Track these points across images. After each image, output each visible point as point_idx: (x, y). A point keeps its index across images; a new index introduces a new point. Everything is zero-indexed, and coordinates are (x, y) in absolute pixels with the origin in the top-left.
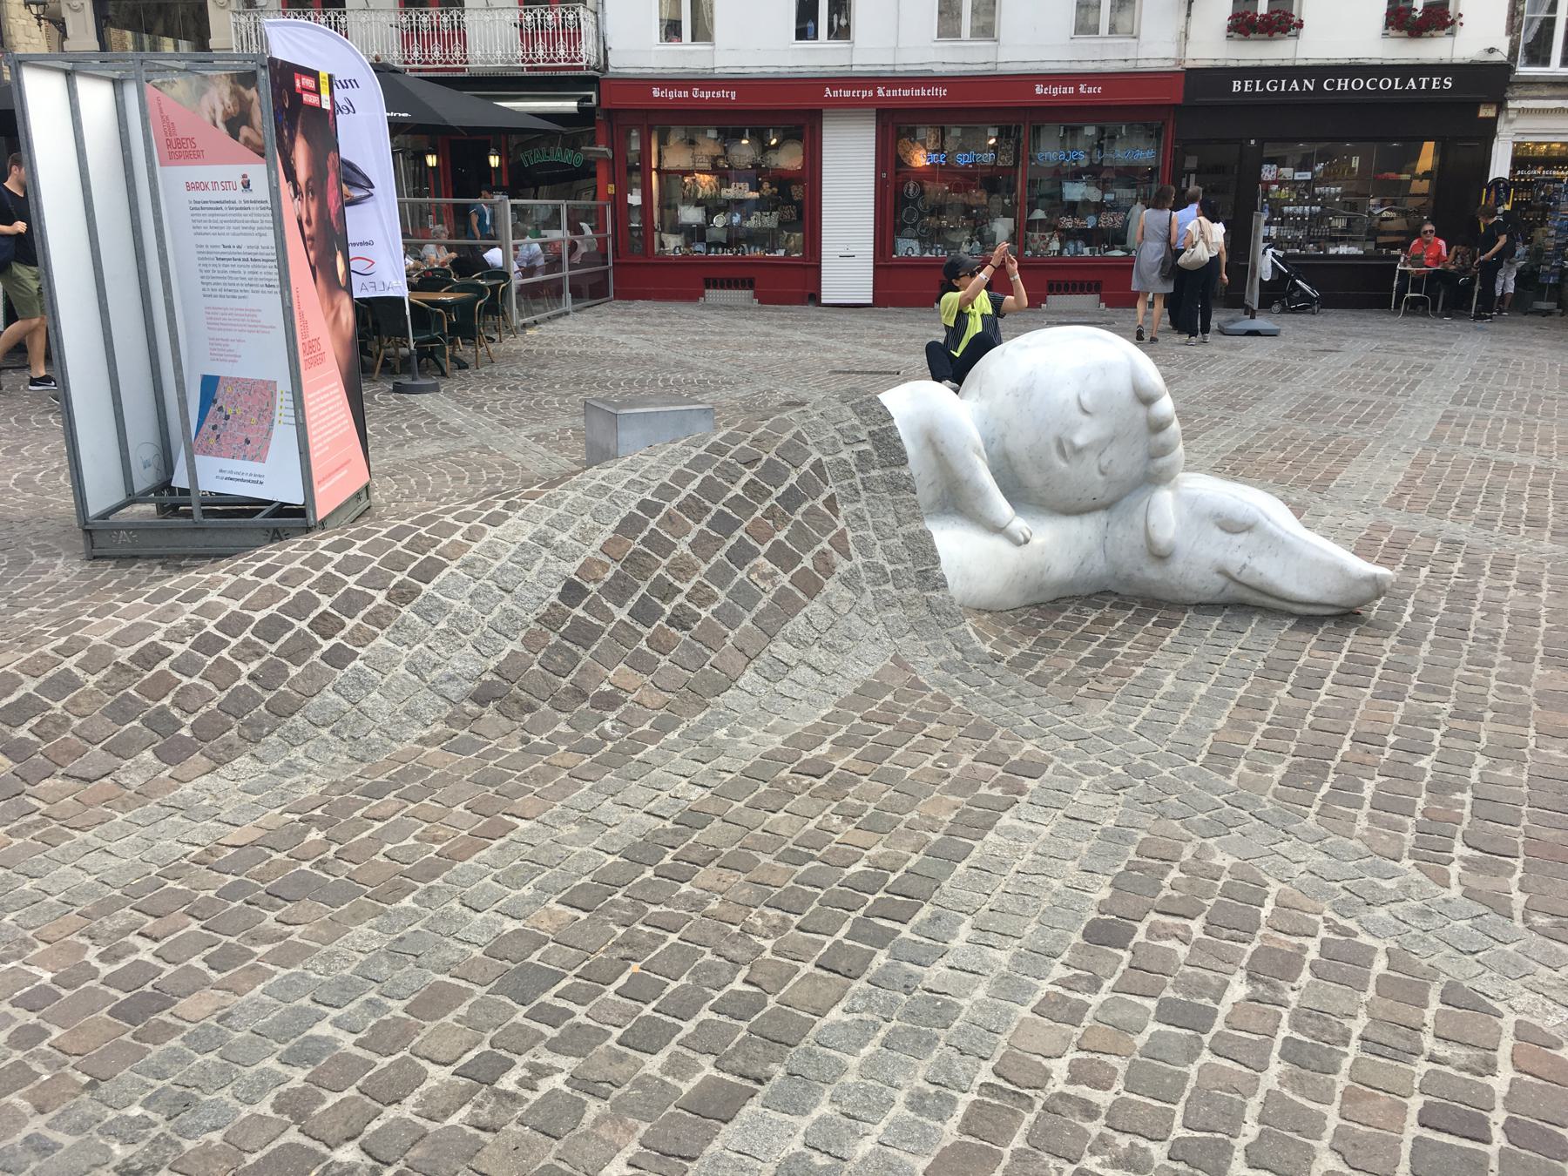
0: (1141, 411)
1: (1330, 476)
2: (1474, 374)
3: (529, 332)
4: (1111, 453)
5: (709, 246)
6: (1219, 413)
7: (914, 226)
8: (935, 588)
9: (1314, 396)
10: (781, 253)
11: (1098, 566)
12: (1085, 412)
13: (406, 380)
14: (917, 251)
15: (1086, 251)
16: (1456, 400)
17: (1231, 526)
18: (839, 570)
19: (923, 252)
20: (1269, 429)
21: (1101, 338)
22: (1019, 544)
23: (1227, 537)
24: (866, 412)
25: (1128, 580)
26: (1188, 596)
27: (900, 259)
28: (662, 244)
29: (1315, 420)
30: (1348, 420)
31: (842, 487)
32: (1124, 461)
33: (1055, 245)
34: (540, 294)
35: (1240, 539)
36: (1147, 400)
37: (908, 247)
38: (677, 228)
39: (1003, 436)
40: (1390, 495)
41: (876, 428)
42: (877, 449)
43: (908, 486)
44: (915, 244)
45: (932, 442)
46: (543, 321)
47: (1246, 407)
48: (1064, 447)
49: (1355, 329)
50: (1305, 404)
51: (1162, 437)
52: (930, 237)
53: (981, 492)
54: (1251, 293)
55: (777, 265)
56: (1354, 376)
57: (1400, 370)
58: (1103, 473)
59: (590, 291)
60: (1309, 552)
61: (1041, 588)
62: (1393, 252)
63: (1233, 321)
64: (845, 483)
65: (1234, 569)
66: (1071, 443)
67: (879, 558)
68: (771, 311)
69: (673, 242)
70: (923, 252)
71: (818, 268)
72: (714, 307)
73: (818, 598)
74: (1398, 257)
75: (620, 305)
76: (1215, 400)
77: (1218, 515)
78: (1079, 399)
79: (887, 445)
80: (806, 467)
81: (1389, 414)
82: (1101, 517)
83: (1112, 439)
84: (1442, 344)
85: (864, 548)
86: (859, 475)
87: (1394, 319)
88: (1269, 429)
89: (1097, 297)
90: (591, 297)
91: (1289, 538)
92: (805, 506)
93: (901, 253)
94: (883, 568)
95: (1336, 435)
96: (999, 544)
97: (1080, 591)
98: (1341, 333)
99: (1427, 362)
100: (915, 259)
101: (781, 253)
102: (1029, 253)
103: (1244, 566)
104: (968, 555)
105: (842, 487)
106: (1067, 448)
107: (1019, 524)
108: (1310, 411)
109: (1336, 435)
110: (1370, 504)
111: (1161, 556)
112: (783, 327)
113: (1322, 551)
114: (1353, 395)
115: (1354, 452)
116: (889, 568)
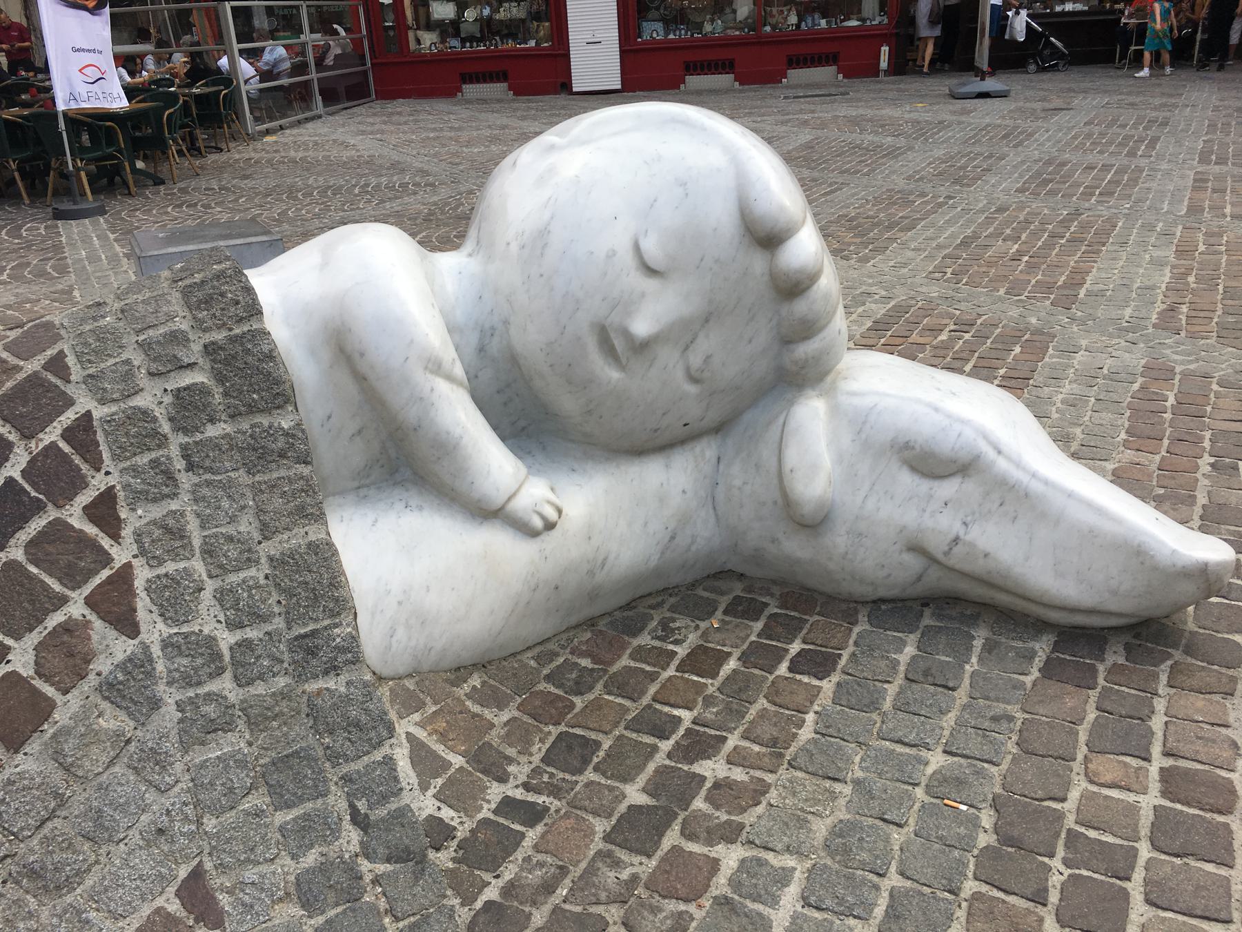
0: (758, 263)
1: (1076, 280)
2: (1212, 127)
3: (268, 139)
4: (706, 344)
5: (463, 41)
6: (943, 191)
7: (657, 9)
8: (332, 669)
9: (1049, 163)
10: (532, 43)
11: (704, 534)
12: (650, 271)
13: (66, 206)
14: (662, 33)
15: (823, 23)
16: (1204, 160)
17: (930, 463)
18: (102, 665)
19: (667, 34)
20: (1000, 210)
21: (686, 123)
22: (533, 533)
23: (924, 485)
24: (207, 302)
25: (757, 557)
26: (860, 590)
27: (645, 42)
28: (418, 42)
29: (1052, 193)
30: (1088, 194)
31: (135, 471)
32: (733, 353)
33: (793, 19)
34: (286, 99)
35: (948, 489)
36: (767, 238)
37: (653, 31)
38: (430, 25)
39: (506, 322)
40: (1159, 307)
41: (219, 336)
42: (220, 378)
43: (296, 447)
44: (659, 26)
45: (343, 347)
46: (292, 126)
47: (976, 179)
48: (609, 340)
49: (1082, 85)
50: (1039, 173)
51: (800, 307)
52: (675, 19)
53: (447, 448)
54: (981, 56)
55: (527, 56)
56: (1089, 136)
57: (1135, 126)
58: (694, 380)
59: (345, 92)
60: (1075, 506)
61: (593, 595)
62: (1117, 6)
63: (964, 84)
64: (143, 460)
65: (937, 546)
66: (626, 334)
67: (209, 621)
68: (523, 103)
69: (428, 39)
70: (667, 34)
71: (566, 56)
72: (469, 102)
73: (34, 746)
74: (1122, 12)
75: (378, 106)
76: (940, 174)
77: (907, 446)
78: (637, 248)
79: (249, 370)
80: (52, 435)
81: (1134, 181)
82: (707, 450)
83: (707, 319)
84: (1171, 96)
85: (174, 599)
86: (177, 441)
87: (1119, 73)
88: (1000, 210)
89: (834, 68)
90: (349, 99)
91: (1036, 486)
92: (36, 525)
93: (646, 37)
94: (211, 641)
95: (1077, 213)
96: (496, 542)
97: (675, 580)
98: (1070, 90)
99: (1161, 115)
100: (660, 42)
101: (532, 43)
102: (768, 29)
103: (956, 540)
104: (407, 574)
105: (135, 471)
106: (619, 344)
107: (534, 492)
108: (1046, 182)
109: (1077, 213)
110: (1134, 326)
111: (813, 524)
112: (523, 118)
113: (1100, 511)
114: (1091, 158)
115: (1102, 236)
116: (226, 639)
